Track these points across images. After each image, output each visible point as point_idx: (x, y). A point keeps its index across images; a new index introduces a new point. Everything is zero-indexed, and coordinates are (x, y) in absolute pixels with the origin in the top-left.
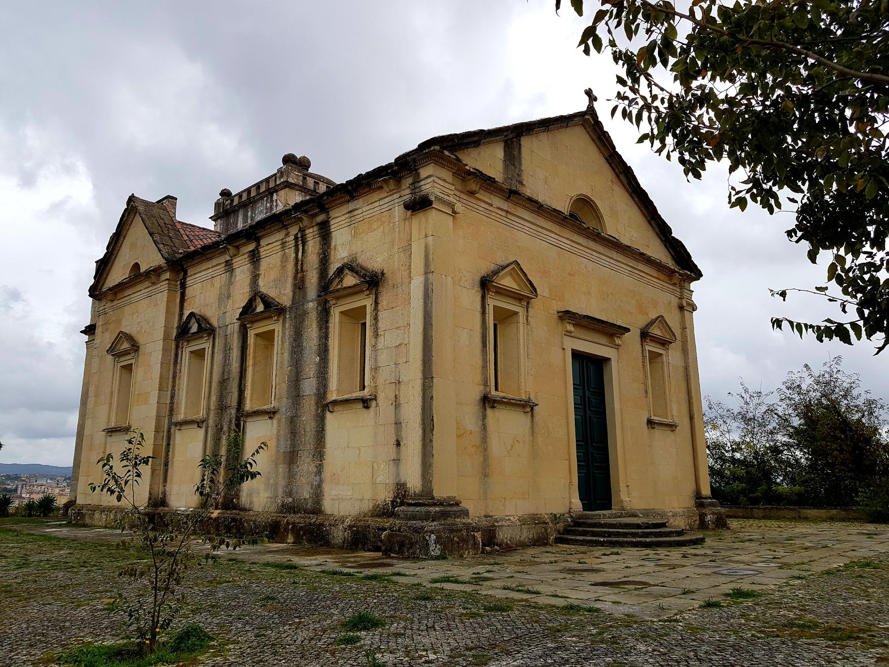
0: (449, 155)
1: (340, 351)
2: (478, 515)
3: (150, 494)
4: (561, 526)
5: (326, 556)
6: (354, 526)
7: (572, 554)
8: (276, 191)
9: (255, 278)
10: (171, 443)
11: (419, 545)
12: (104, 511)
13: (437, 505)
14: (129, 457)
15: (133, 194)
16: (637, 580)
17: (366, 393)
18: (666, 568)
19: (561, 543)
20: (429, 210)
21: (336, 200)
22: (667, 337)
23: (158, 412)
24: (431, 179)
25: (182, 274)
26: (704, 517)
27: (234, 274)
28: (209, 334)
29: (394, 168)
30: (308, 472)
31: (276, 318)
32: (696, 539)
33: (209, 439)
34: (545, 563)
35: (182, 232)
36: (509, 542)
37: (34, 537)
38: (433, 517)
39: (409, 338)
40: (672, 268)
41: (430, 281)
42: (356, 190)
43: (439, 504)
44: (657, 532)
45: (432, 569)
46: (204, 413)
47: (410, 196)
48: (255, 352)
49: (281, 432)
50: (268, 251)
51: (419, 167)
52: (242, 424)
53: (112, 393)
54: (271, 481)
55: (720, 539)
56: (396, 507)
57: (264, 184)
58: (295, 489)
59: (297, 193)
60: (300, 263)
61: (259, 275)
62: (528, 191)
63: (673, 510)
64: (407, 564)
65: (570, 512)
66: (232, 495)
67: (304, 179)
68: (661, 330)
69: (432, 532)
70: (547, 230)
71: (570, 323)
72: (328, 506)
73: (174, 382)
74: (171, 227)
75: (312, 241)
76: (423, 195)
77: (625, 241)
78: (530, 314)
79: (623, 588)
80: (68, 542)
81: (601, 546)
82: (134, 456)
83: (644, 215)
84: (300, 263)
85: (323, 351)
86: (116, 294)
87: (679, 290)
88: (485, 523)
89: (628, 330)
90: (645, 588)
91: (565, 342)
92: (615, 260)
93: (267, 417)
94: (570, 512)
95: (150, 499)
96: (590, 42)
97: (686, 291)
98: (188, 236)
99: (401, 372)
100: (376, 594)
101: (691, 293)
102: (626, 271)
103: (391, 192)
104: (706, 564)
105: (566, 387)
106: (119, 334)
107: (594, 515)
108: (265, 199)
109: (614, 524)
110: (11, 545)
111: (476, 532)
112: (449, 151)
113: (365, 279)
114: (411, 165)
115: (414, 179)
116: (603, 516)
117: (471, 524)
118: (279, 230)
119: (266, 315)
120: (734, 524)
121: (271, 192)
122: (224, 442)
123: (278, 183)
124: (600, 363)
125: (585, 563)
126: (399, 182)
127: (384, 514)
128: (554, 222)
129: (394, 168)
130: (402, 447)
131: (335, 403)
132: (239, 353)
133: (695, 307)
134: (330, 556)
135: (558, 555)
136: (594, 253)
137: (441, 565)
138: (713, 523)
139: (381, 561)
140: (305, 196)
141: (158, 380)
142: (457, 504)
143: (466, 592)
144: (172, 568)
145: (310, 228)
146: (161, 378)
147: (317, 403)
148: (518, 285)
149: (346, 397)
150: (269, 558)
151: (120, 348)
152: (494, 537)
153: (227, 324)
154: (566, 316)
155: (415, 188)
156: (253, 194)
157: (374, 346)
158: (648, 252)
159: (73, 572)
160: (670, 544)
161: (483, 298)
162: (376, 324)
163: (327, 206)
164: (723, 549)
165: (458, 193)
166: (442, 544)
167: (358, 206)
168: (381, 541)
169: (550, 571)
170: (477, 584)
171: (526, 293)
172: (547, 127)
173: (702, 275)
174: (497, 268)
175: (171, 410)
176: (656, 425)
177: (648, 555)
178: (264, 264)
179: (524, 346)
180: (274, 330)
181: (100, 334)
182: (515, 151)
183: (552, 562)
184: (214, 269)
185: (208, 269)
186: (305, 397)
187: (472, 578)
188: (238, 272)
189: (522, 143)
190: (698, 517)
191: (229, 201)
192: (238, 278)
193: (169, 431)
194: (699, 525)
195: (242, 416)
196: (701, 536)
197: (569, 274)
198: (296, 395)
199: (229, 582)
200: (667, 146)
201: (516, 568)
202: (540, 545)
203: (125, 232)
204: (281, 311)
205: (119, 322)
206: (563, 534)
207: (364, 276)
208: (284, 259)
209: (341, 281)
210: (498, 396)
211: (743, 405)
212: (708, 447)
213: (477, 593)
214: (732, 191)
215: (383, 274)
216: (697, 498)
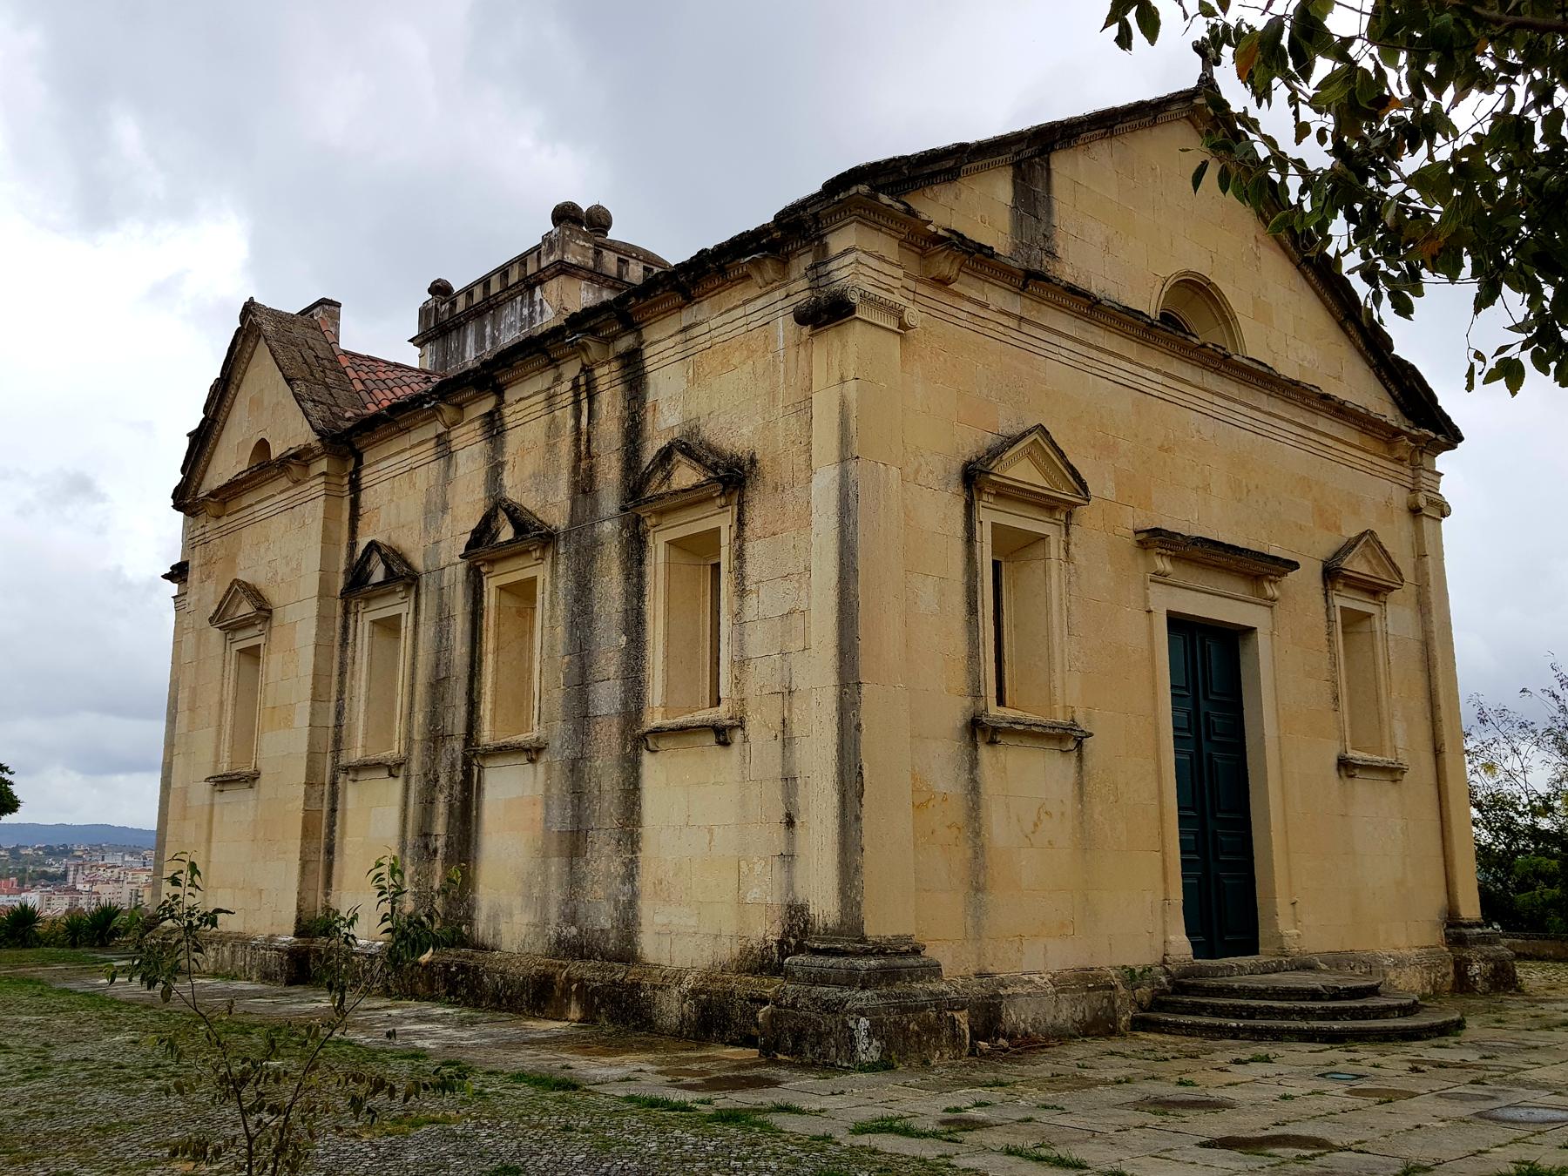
0: (890, 202)
1: (667, 625)
2: (962, 972)
3: (299, 910)
4: (1144, 993)
5: (643, 1057)
6: (701, 991)
7: (1166, 1059)
8: (541, 282)
9: (495, 470)
10: (339, 807)
11: (835, 1040)
12: (211, 943)
13: (873, 955)
14: (175, 912)
15: (252, 299)
16: (1303, 1133)
17: (722, 713)
18: (1373, 1100)
19: (1144, 1030)
20: (848, 324)
21: (655, 305)
22: (1384, 576)
23: (311, 745)
24: (851, 258)
25: (353, 461)
26: (1466, 966)
27: (454, 462)
28: (408, 587)
29: (775, 235)
30: (609, 875)
31: (538, 552)
32: (1445, 1023)
33: (412, 801)
34: (1105, 1083)
35: (352, 374)
36: (1030, 1030)
37: (72, 998)
38: (863, 980)
39: (809, 597)
40: (1394, 424)
41: (852, 477)
42: (695, 283)
43: (877, 953)
44: (1356, 1008)
45: (860, 1096)
46: (402, 748)
47: (808, 293)
48: (498, 625)
49: (554, 791)
50: (520, 415)
51: (826, 231)
52: (476, 772)
53: (221, 703)
54: (536, 892)
55: (1499, 1021)
56: (788, 955)
57: (516, 267)
58: (582, 907)
59: (583, 284)
60: (584, 438)
61: (501, 465)
62: (1068, 270)
63: (1395, 952)
64: (809, 1081)
65: (1165, 961)
66: (460, 918)
67: (598, 253)
68: (1369, 562)
69: (861, 1013)
70: (1111, 354)
71: (1162, 555)
72: (650, 946)
73: (342, 683)
74: (329, 366)
75: (609, 392)
76: (834, 293)
77: (1287, 370)
78: (1074, 538)
79: (1270, 1156)
80: (137, 1011)
81: (1232, 1038)
82: (186, 911)
83: (1329, 309)
84: (584, 438)
85: (635, 623)
86: (224, 503)
87: (1409, 472)
88: (977, 989)
89: (1294, 565)
90: (1321, 1155)
91: (1151, 597)
92: (1265, 413)
93: (524, 759)
94: (1165, 961)
95: (299, 921)
96: (1131, 17)
97: (1425, 474)
98: (363, 383)
99: (793, 671)
100: (733, 1162)
101: (1435, 478)
102: (1290, 436)
103: (768, 287)
104: (1461, 1090)
105: (1155, 694)
106: (232, 585)
107: (1219, 968)
108: (519, 298)
109: (1262, 990)
110: (25, 1018)
111: (958, 1010)
112: (891, 194)
113: (716, 473)
114: (810, 227)
115: (816, 257)
116: (1238, 970)
117: (947, 993)
118: (541, 370)
119: (519, 547)
120: (1532, 976)
121: (530, 284)
122: (441, 808)
123: (544, 264)
124: (1232, 639)
125: (1193, 1084)
126: (784, 262)
127: (762, 968)
128: (1126, 335)
129: (775, 235)
130: (799, 830)
131: (659, 732)
132: (467, 625)
133: (1446, 509)
134: (651, 1056)
135: (1135, 1062)
136: (1217, 400)
137: (879, 1085)
138: (1486, 980)
139: (755, 1071)
140: (600, 290)
141: (309, 680)
142: (916, 952)
143: (925, 1160)
144: (281, 1138)
145: (602, 365)
146: (316, 675)
147: (623, 732)
148: (1047, 476)
149: (682, 720)
150: (526, 1060)
151: (234, 613)
152: (998, 1018)
153: (442, 564)
154: (1155, 539)
155: (818, 277)
156: (495, 288)
157: (738, 615)
158: (1340, 392)
159: (128, 1092)
160: (1386, 1036)
161: (969, 508)
162: (741, 567)
163: (636, 319)
164: (1504, 1049)
165: (911, 284)
166: (883, 1037)
167: (700, 318)
168: (757, 1025)
169: (1115, 1106)
170: (949, 1140)
171: (1065, 494)
172: (1108, 128)
173: (1461, 439)
174: (998, 442)
175: (338, 741)
176: (1357, 771)
177: (1333, 1063)
178: (512, 440)
179: (1061, 609)
180: (534, 579)
181: (195, 583)
182: (1036, 186)
183: (1119, 1082)
184: (414, 452)
185: (403, 451)
186: (600, 719)
187: (943, 1122)
188: (461, 457)
189: (1052, 166)
190: (1451, 968)
191: (447, 305)
192: (461, 471)
193: (334, 783)
194: (1454, 983)
195: (474, 756)
196: (1457, 1016)
197: (1161, 448)
198: (581, 715)
199: (435, 1122)
200: (1335, 240)
201: (1042, 1095)
202: (1099, 1035)
203: (239, 377)
204: (548, 539)
205: (231, 559)
206: (1150, 1010)
207: (714, 467)
208: (553, 430)
209: (668, 477)
210: (1003, 718)
211: (1555, 713)
212: (1478, 806)
213: (949, 1165)
214: (1475, 361)
215: (753, 462)
216: (1449, 926)
